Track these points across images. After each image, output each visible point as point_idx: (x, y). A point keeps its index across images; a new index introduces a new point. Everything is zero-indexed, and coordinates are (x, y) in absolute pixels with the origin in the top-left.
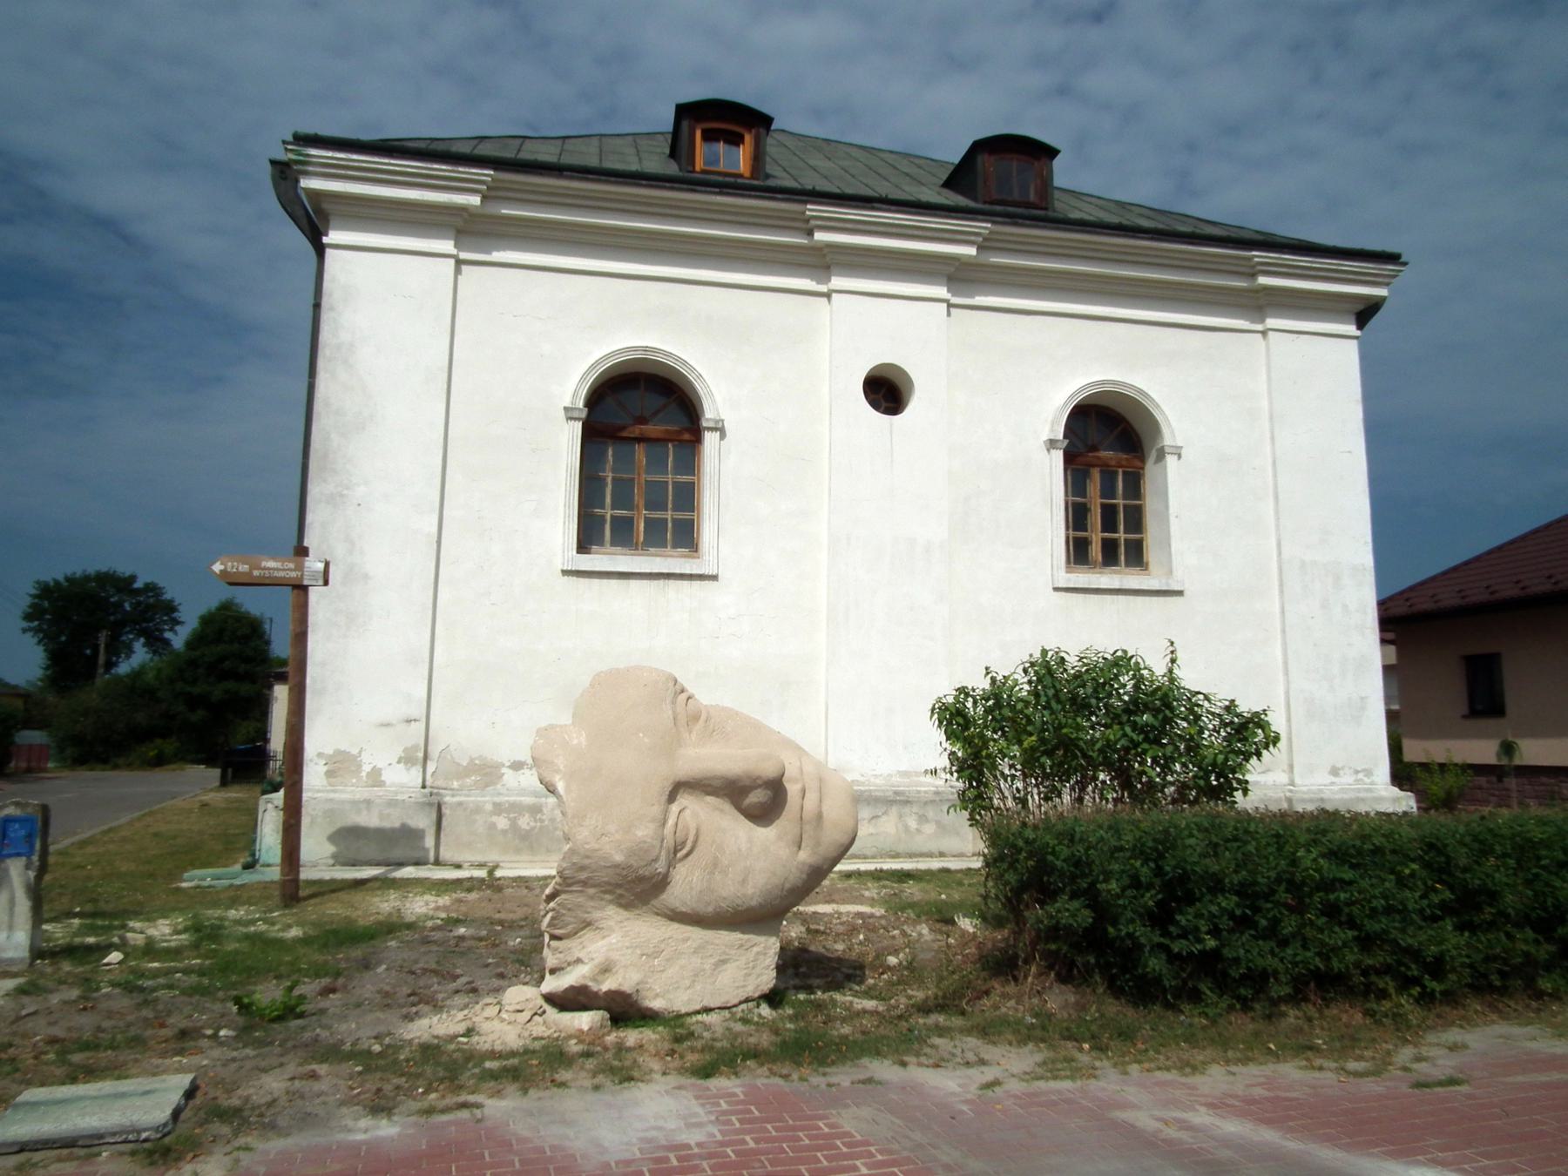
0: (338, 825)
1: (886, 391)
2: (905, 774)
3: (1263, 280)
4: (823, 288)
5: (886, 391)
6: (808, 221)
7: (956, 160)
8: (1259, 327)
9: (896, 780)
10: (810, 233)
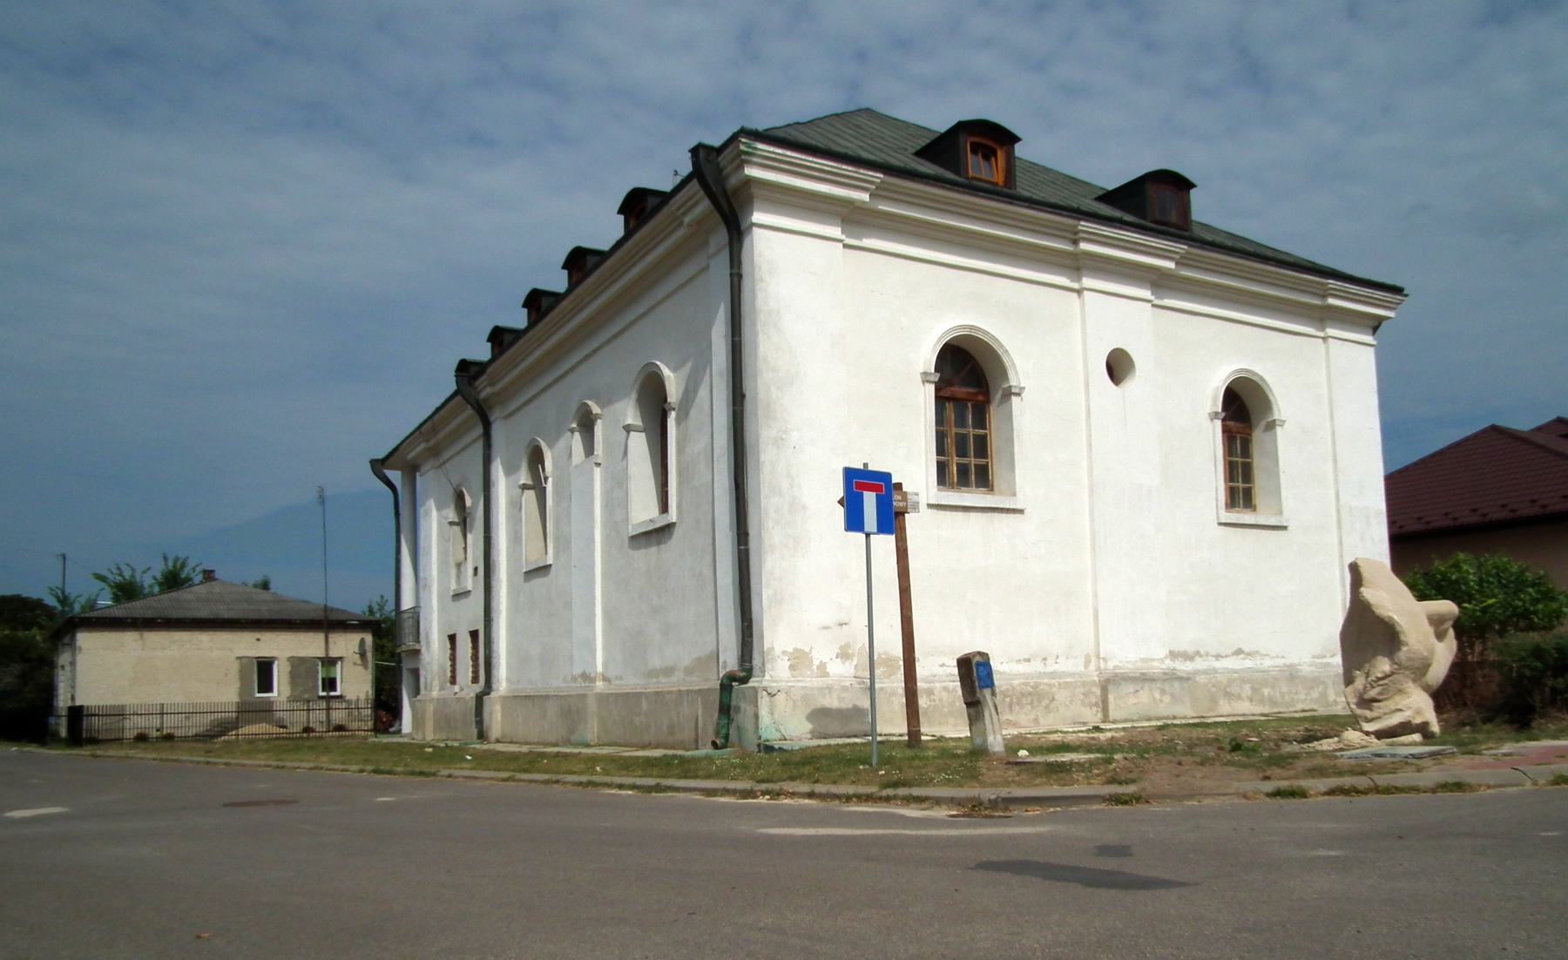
0: (812, 707)
1: (1118, 367)
2: (1143, 660)
3: (1331, 301)
4: (1076, 286)
5: (1118, 367)
6: (1076, 233)
7: (943, 130)
8: (1321, 334)
9: (1140, 664)
10: (1075, 242)
